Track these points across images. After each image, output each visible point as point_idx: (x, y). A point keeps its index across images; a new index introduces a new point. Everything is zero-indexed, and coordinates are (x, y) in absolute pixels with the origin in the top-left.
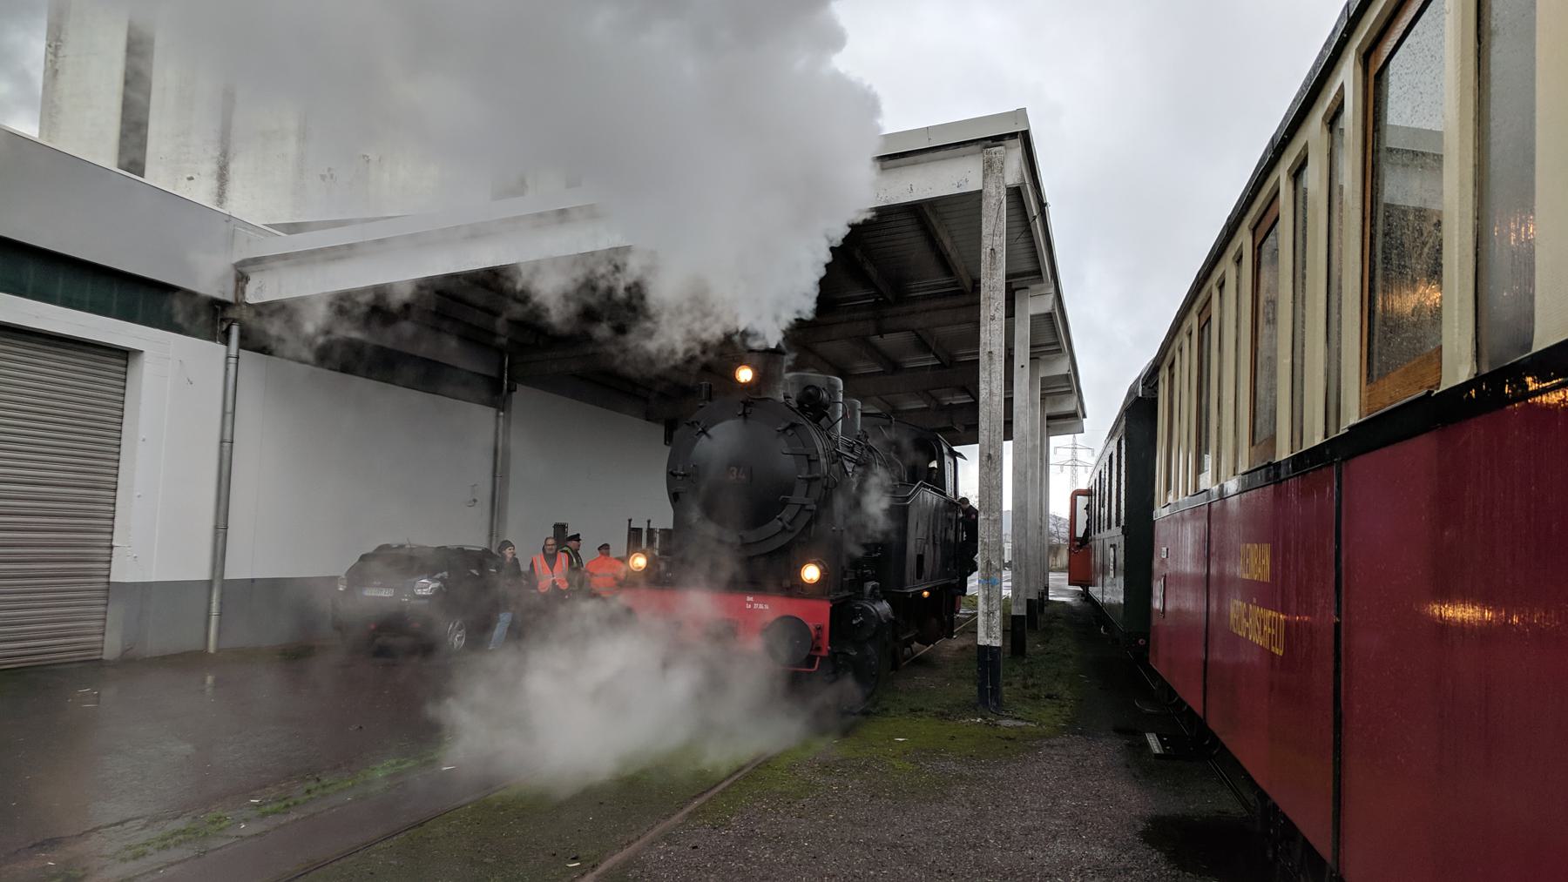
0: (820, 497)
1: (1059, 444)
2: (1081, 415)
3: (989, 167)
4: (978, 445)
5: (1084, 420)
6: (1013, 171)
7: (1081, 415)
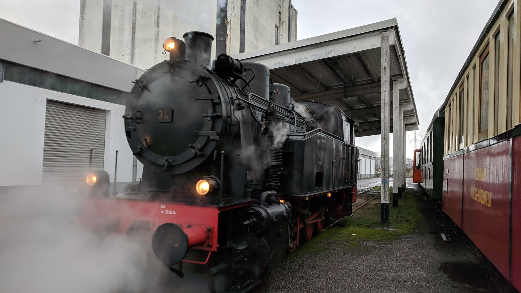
3: (383, 39)
6: (392, 39)
7: (417, 123)
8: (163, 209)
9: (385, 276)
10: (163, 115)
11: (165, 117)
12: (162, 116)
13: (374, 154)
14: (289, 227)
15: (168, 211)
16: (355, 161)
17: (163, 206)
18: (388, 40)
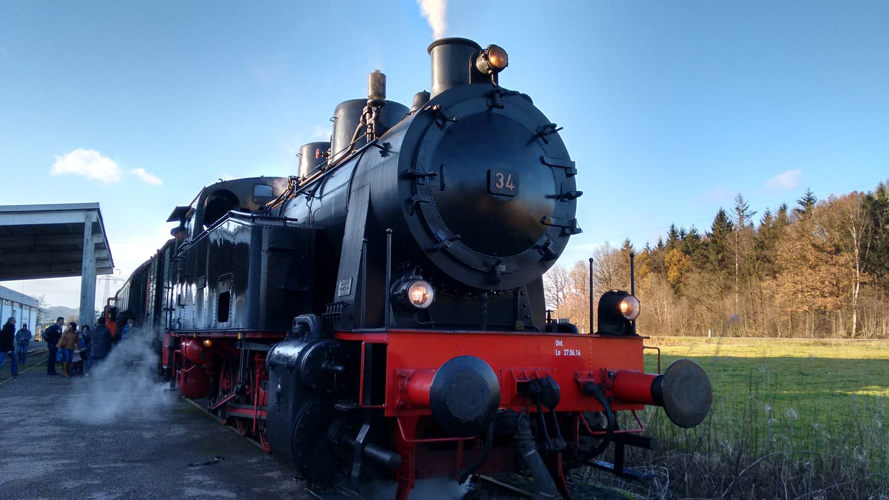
0: (283, 195)
1: (101, 279)
2: (112, 266)
3: (87, 217)
4: (79, 279)
5: (114, 268)
6: (94, 217)
7: (112, 266)
8: (559, 348)
9: (736, 495)
10: (505, 182)
11: (507, 186)
12: (502, 184)
13: (36, 301)
14: (68, 357)
15: (568, 350)
16: (170, 288)
17: (559, 343)
18: (91, 218)
